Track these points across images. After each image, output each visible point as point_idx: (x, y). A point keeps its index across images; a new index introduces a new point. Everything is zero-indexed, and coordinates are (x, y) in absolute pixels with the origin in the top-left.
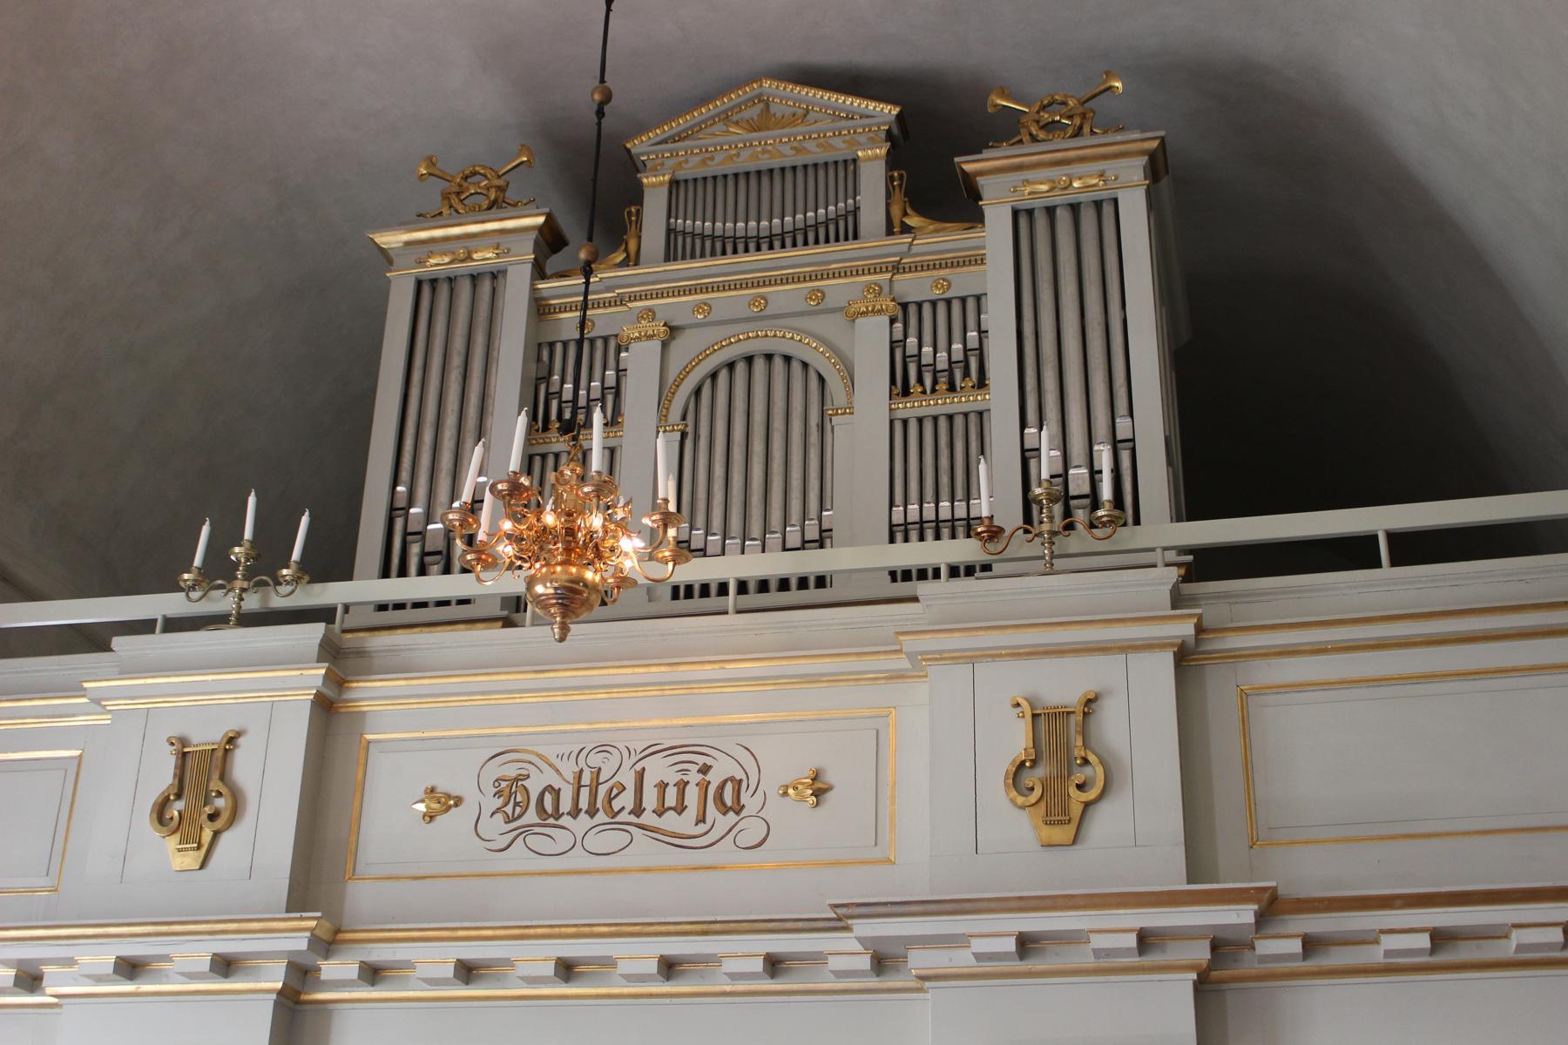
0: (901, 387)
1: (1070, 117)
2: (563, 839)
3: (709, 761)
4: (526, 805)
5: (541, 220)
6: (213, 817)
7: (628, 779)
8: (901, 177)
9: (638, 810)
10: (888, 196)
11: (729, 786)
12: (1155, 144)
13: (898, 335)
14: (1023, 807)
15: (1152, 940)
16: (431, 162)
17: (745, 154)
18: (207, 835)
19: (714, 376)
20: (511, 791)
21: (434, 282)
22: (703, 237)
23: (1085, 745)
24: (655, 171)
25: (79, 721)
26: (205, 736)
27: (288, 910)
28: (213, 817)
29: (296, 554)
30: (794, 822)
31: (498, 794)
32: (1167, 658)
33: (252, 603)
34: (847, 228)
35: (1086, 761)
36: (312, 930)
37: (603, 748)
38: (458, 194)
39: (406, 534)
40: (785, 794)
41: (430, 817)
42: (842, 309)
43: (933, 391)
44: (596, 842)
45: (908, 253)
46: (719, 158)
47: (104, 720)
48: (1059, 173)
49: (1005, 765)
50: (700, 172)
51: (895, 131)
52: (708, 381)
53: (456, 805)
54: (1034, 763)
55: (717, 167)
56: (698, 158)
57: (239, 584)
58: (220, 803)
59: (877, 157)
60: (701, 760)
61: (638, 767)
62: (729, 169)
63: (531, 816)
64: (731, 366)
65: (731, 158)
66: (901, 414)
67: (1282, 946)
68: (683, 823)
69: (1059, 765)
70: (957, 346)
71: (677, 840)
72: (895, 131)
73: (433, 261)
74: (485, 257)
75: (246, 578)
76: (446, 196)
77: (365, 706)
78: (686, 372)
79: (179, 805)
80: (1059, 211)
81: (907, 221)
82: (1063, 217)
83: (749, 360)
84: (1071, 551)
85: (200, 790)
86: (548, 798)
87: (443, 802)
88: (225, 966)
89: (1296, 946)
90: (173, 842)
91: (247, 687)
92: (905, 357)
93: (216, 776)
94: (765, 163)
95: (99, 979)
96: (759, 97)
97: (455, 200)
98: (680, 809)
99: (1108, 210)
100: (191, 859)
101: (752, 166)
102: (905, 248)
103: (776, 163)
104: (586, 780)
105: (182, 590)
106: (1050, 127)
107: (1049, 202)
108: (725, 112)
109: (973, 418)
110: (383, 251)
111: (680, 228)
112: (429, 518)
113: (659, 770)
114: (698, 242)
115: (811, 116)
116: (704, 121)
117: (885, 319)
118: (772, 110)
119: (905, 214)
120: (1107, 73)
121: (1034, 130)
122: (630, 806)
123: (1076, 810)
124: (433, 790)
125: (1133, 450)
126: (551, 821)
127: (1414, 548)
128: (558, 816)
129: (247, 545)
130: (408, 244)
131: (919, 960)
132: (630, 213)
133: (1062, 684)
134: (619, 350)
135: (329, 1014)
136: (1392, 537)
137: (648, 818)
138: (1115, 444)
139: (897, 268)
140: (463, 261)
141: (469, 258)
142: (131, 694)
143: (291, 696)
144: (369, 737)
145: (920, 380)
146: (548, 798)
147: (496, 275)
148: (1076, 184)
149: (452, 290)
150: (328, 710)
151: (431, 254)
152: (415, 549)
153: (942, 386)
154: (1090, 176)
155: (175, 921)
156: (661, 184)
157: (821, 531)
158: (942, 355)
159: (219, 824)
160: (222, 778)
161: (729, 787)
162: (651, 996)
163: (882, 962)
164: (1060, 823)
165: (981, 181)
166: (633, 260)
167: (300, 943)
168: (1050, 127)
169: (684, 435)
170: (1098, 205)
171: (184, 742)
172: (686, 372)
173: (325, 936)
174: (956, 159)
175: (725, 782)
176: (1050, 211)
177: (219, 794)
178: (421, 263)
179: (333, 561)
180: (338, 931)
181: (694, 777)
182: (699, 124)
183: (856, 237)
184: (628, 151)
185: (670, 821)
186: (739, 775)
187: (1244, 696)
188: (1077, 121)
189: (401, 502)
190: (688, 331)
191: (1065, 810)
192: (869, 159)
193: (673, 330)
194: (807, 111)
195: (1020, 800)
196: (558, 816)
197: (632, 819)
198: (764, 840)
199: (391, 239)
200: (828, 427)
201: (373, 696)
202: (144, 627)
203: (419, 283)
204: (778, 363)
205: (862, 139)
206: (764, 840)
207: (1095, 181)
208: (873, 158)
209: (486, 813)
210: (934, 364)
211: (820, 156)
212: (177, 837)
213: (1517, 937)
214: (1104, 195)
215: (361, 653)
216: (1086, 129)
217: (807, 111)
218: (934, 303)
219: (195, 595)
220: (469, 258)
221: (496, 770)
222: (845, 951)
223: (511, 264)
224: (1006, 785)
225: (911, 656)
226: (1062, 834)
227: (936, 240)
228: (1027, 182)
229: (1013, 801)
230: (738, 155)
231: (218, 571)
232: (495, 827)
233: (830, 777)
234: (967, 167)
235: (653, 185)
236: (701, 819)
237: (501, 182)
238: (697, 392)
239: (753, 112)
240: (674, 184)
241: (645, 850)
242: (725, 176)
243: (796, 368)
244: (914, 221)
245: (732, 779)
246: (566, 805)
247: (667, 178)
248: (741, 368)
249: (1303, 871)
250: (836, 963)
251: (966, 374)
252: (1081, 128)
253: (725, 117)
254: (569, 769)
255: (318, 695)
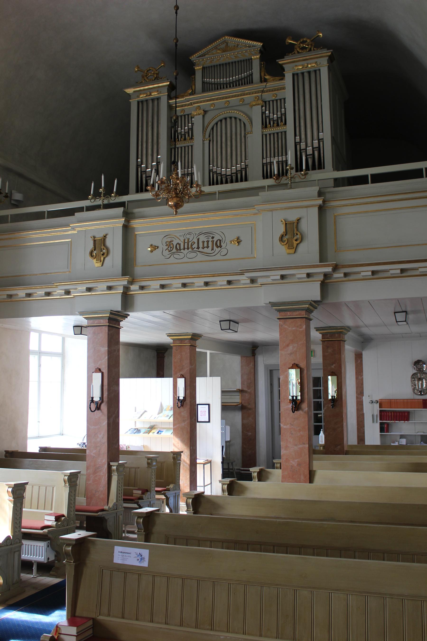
0: (265, 125)
1: (308, 45)
2: (182, 255)
3: (214, 236)
4: (174, 248)
5: (168, 83)
6: (103, 255)
7: (196, 240)
8: (264, 63)
9: (198, 248)
10: (260, 70)
11: (218, 241)
12: (330, 54)
13: (264, 111)
14: (283, 245)
15: (311, 275)
16: (138, 67)
17: (222, 59)
18: (102, 259)
19: (217, 124)
20: (169, 244)
21: (142, 102)
22: (212, 84)
23: (297, 230)
24: (199, 65)
25: (70, 232)
26: (99, 236)
27: (122, 276)
28: (103, 255)
29: (115, 190)
30: (233, 249)
31: (167, 245)
32: (316, 210)
33: (106, 202)
34: (249, 80)
35: (297, 234)
36: (128, 280)
37: (190, 234)
38: (146, 76)
39: (141, 172)
40: (231, 243)
41: (152, 251)
42: (249, 104)
43: (273, 126)
44: (189, 255)
45: (265, 87)
46: (215, 60)
47: (75, 232)
48: (305, 63)
49: (279, 235)
50: (210, 65)
51: (262, 49)
52: (215, 125)
53: (157, 248)
54: (286, 235)
55: (215, 62)
56: (209, 61)
57: (102, 198)
58: (104, 251)
59: (257, 58)
60: (212, 235)
61: (198, 238)
62: (218, 63)
63: (174, 250)
64: (221, 121)
65: (218, 60)
66: (265, 133)
67: (339, 275)
68: (209, 250)
69: (292, 234)
70: (279, 113)
71: (207, 254)
72: (262, 49)
73: (141, 96)
74: (155, 94)
75: (104, 196)
76: (143, 77)
77: (135, 226)
78: (209, 123)
79: (95, 252)
80: (305, 73)
81: (266, 77)
82: (306, 75)
83: (226, 119)
84: (297, 181)
85: (99, 248)
86: (178, 246)
87: (154, 248)
88: (110, 288)
89: (342, 275)
90: (95, 261)
91: (108, 224)
92: (266, 117)
93: (102, 245)
94: (227, 61)
95: (83, 292)
96: (225, 41)
97: (145, 78)
98: (208, 247)
99: (318, 72)
100: (99, 264)
101: (224, 62)
102: (264, 86)
103: (230, 61)
104: (186, 241)
105: (89, 199)
106: (303, 48)
107: (303, 71)
108: (216, 46)
109: (283, 133)
110: (128, 94)
111: (206, 82)
112: (147, 167)
113: (202, 238)
114: (211, 85)
115: (239, 46)
116: (210, 50)
117: (260, 106)
118: (229, 44)
119: (265, 75)
120: (318, 31)
121: (298, 50)
122: (196, 247)
123: (295, 245)
124: (152, 245)
125: (323, 142)
126: (179, 251)
127: (378, 178)
128: (180, 250)
129: (103, 188)
130: (134, 92)
131: (260, 281)
132: (192, 78)
133: (292, 216)
134: (192, 118)
135: (134, 296)
136: (372, 175)
137: (201, 249)
138: (319, 140)
139: (263, 92)
140: (149, 96)
141: (151, 95)
142: (81, 226)
143: (117, 225)
144: (136, 233)
145: (270, 123)
146: (178, 246)
147: (158, 99)
148: (309, 66)
149: (147, 104)
150: (126, 228)
151: (141, 94)
152: (144, 176)
153: (275, 125)
154: (313, 63)
155: (98, 279)
156: (200, 69)
157: (246, 166)
158: (275, 116)
159: (105, 256)
160: (104, 245)
161: (218, 242)
162: (203, 290)
163: (253, 281)
164: (291, 249)
165: (284, 66)
166: (193, 93)
167: (125, 283)
168: (303, 48)
169: (210, 141)
170: (315, 71)
171: (94, 237)
172: (209, 123)
173: (131, 281)
174: (277, 61)
175: (217, 240)
176: (303, 73)
177: (104, 249)
178: (138, 97)
179: (124, 190)
180: (133, 279)
181: (211, 240)
182: (209, 50)
183: (252, 83)
184: (191, 60)
185: (206, 250)
186: (221, 239)
187: (335, 216)
188: (310, 47)
189: (139, 164)
190: (209, 112)
191: (293, 246)
192: (255, 59)
193: (205, 112)
194: (238, 45)
195: (283, 243)
196: (180, 250)
197: (197, 250)
198: (226, 255)
199: (129, 91)
200: (247, 137)
201: (136, 224)
202: (81, 210)
203: (138, 102)
204: (233, 119)
205: (253, 53)
206: (226, 255)
207: (314, 65)
208: (256, 57)
209: (164, 250)
210: (273, 118)
211: (242, 58)
212: (95, 260)
213: (391, 272)
214: (317, 69)
215: (133, 213)
216: (312, 49)
217: (238, 45)
218: (273, 101)
219: (92, 201)
220: (151, 95)
221: (166, 240)
222: (244, 279)
223: (162, 96)
224: (279, 240)
225: (258, 210)
226: (292, 251)
227: (273, 84)
228: (296, 66)
229: (281, 243)
230: (220, 59)
231: (97, 195)
232: (166, 253)
233: (241, 238)
234: (280, 63)
235: (198, 69)
236: (213, 249)
237: (157, 72)
238: (213, 128)
239: (223, 46)
240: (204, 68)
241: (200, 257)
242: (217, 65)
243: (238, 121)
244: (267, 77)
245: (219, 240)
246: (182, 247)
247: (201, 67)
248: (224, 121)
249: (347, 257)
250: (242, 282)
251: (282, 121)
252: (311, 48)
253: (216, 48)
254: (182, 239)
255: (123, 225)
